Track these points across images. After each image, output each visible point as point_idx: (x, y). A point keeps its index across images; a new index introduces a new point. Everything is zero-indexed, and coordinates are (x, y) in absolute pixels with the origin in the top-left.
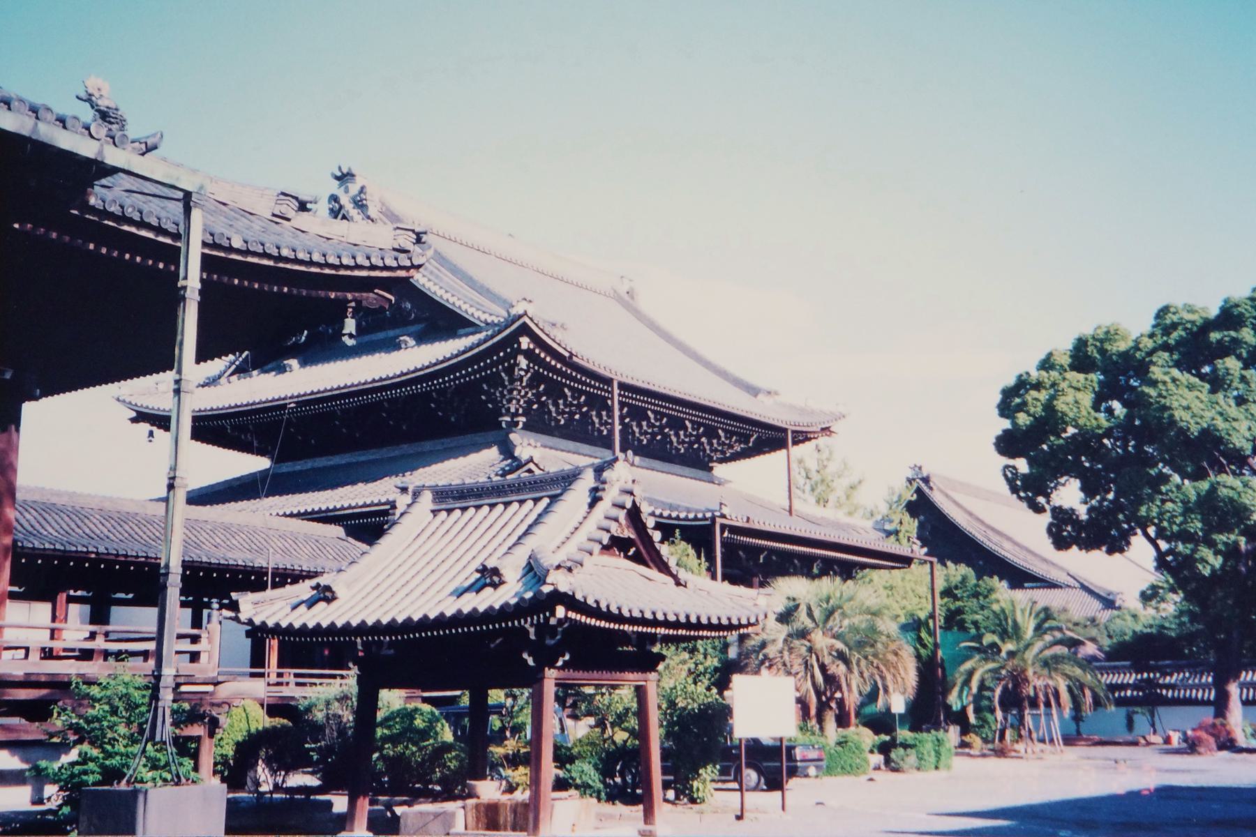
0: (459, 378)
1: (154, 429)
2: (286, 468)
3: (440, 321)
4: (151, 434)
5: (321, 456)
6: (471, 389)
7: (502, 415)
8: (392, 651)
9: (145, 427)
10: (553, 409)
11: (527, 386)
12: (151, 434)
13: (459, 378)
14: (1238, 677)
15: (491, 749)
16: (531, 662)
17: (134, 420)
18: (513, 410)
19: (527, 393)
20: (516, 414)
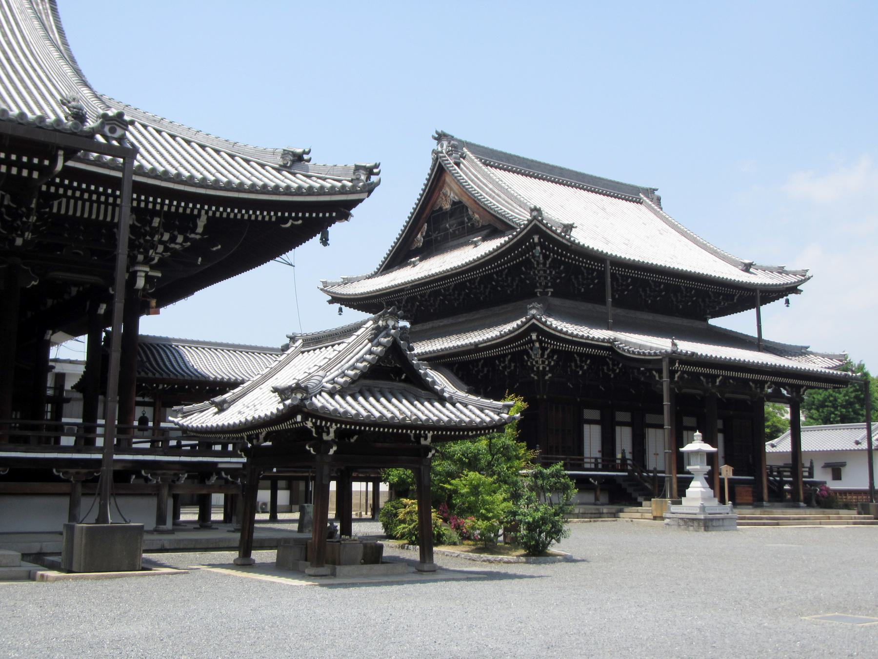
0: (580, 262)
1: (343, 307)
2: (418, 327)
3: (495, 225)
4: (341, 310)
5: (437, 319)
6: (514, 270)
7: (537, 288)
8: (269, 443)
9: (337, 306)
10: (575, 282)
11: (549, 268)
12: (341, 310)
13: (576, 261)
14: (500, 420)
15: (698, 433)
16: (355, 437)
17: (330, 302)
18: (543, 284)
19: (551, 272)
20: (546, 287)
